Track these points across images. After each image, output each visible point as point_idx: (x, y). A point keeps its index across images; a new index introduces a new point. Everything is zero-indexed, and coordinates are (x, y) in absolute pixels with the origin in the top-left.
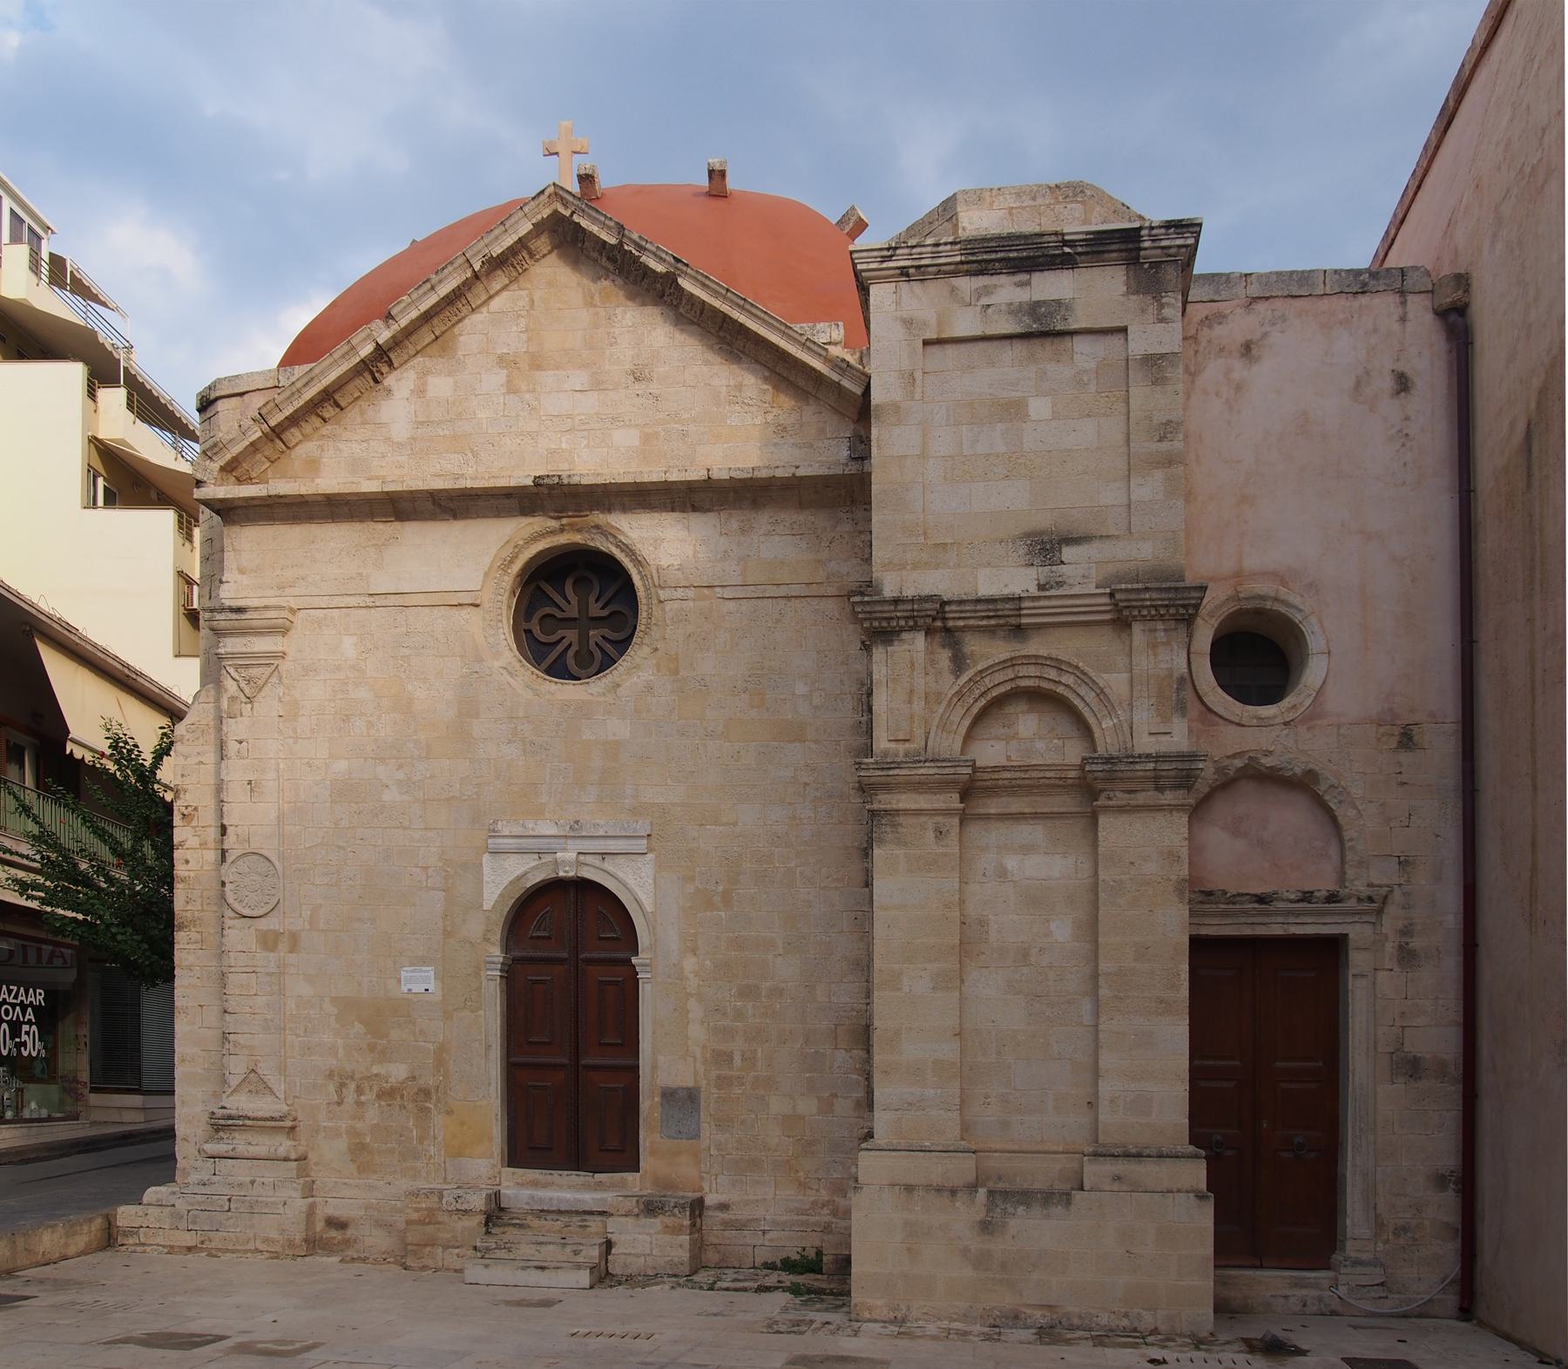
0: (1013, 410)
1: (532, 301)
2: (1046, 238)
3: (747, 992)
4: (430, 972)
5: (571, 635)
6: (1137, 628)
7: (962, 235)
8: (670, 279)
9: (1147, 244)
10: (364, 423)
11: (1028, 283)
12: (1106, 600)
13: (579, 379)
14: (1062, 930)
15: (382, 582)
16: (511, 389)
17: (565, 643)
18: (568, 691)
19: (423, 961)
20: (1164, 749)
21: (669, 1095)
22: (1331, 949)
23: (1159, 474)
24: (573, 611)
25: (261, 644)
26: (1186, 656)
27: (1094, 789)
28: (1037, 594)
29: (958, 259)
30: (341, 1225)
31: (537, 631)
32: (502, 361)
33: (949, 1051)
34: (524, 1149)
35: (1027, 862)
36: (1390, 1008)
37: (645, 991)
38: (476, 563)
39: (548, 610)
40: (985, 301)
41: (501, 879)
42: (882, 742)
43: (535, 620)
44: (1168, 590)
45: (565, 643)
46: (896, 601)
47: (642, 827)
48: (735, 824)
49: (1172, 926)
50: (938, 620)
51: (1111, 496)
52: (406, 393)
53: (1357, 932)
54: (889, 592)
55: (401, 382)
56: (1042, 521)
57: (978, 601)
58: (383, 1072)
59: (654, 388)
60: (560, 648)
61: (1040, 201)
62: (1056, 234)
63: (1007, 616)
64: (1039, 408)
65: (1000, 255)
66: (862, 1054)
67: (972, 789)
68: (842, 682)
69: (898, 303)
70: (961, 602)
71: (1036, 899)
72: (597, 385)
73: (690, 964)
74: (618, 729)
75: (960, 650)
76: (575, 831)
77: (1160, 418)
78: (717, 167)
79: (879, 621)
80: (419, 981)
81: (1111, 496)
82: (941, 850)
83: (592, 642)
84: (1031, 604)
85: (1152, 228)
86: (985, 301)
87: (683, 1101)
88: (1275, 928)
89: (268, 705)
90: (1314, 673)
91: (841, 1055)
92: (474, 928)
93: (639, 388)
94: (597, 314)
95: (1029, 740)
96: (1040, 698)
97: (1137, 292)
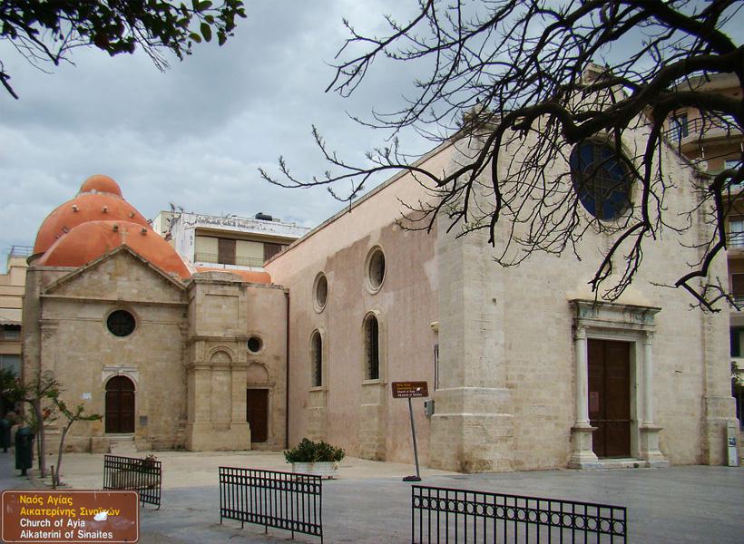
0: (220, 307)
3: (157, 397)
4: (89, 394)
5: (117, 326)
8: (147, 264)
13: (125, 279)
14: (226, 389)
15: (80, 315)
16: (110, 279)
18: (121, 339)
21: (141, 417)
22: (266, 391)
25: (52, 327)
26: (245, 347)
27: (231, 367)
30: (71, 447)
32: (109, 274)
33: (208, 408)
34: (394, 385)
35: (221, 377)
36: (275, 401)
37: (136, 398)
38: (101, 314)
41: (105, 377)
47: (136, 366)
49: (244, 388)
51: (235, 322)
53: (271, 389)
55: (86, 276)
63: (218, 340)
64: (224, 307)
67: (212, 367)
71: (221, 384)
72: (129, 280)
74: (131, 347)
76: (122, 367)
80: (87, 396)
81: (235, 322)
87: (144, 419)
88: (257, 388)
89: (53, 339)
90: (264, 348)
92: (100, 386)
95: (221, 358)
96: (222, 352)
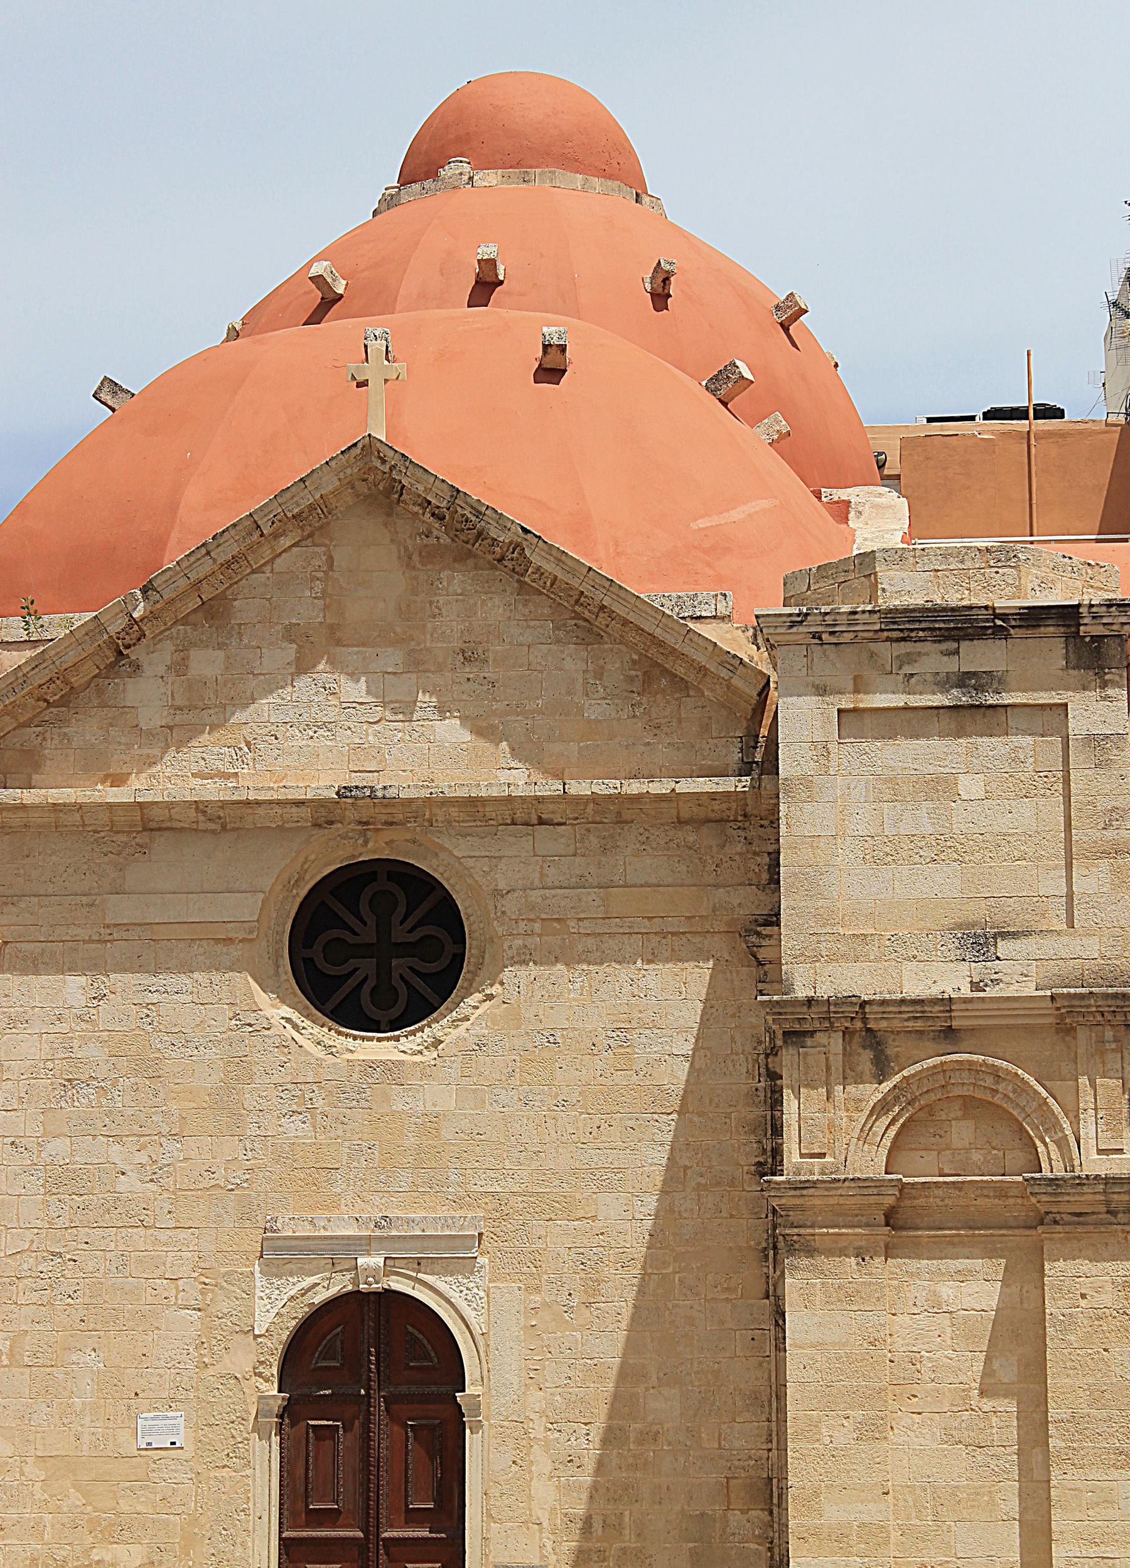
0: (941, 788)
1: (331, 559)
2: (974, 612)
5: (367, 966)
6: (1082, 1034)
7: (882, 603)
9: (1086, 621)
10: (102, 705)
11: (957, 652)
12: (1049, 1004)
17: (359, 976)
19: (171, 1403)
20: (1115, 1171)
23: (1104, 864)
24: (369, 935)
28: (970, 995)
29: (877, 627)
31: (320, 962)
32: (290, 634)
39: (335, 933)
40: (908, 670)
42: (792, 1156)
43: (318, 946)
44: (1115, 996)
45: (359, 976)
46: (810, 1002)
48: (594, 1218)
50: (867, 1032)
52: (161, 670)
54: (802, 992)
56: (976, 912)
57: (903, 1001)
58: (108, 1558)
59: (490, 672)
60: (352, 983)
61: (968, 564)
62: (986, 607)
63: (940, 1022)
64: (970, 786)
65: (923, 625)
66: (764, 1516)
68: (732, 1039)
69: (809, 667)
70: (884, 1002)
73: (536, 1399)
75: (882, 1051)
77: (1104, 804)
78: (555, 341)
79: (797, 1027)
82: (867, 1279)
83: (395, 975)
84: (963, 1006)
85: (1092, 606)
86: (908, 670)
91: (736, 1518)
92: (242, 1360)
93: (471, 671)
94: (416, 578)
97: (1077, 667)
